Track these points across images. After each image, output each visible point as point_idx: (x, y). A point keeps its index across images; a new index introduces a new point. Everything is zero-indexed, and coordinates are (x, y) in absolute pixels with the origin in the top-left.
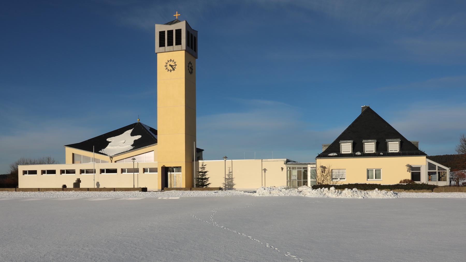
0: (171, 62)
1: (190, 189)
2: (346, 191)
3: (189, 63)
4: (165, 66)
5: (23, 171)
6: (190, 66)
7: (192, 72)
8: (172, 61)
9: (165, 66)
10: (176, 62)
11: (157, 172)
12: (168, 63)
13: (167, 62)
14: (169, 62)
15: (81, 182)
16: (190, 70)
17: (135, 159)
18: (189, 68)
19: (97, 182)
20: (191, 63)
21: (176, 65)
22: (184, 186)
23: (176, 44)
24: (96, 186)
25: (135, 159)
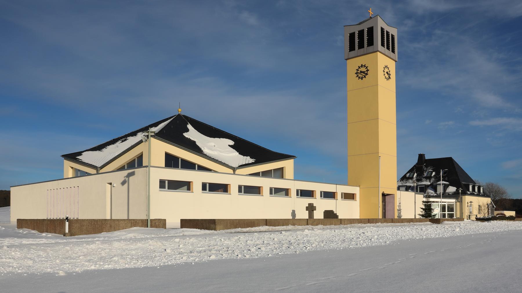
0: (362, 67)
1: (146, 226)
2: (233, 232)
3: (384, 67)
4: (357, 70)
5: (181, 220)
6: (386, 70)
7: (390, 78)
8: (363, 67)
9: (357, 70)
10: (368, 67)
11: (151, 135)
12: (359, 69)
13: (358, 69)
14: (360, 68)
15: (315, 210)
16: (386, 75)
17: (472, 202)
18: (385, 73)
19: (292, 210)
20: (387, 67)
21: (368, 70)
22: (292, 178)
23: (354, 33)
24: (292, 217)
25: (472, 202)
